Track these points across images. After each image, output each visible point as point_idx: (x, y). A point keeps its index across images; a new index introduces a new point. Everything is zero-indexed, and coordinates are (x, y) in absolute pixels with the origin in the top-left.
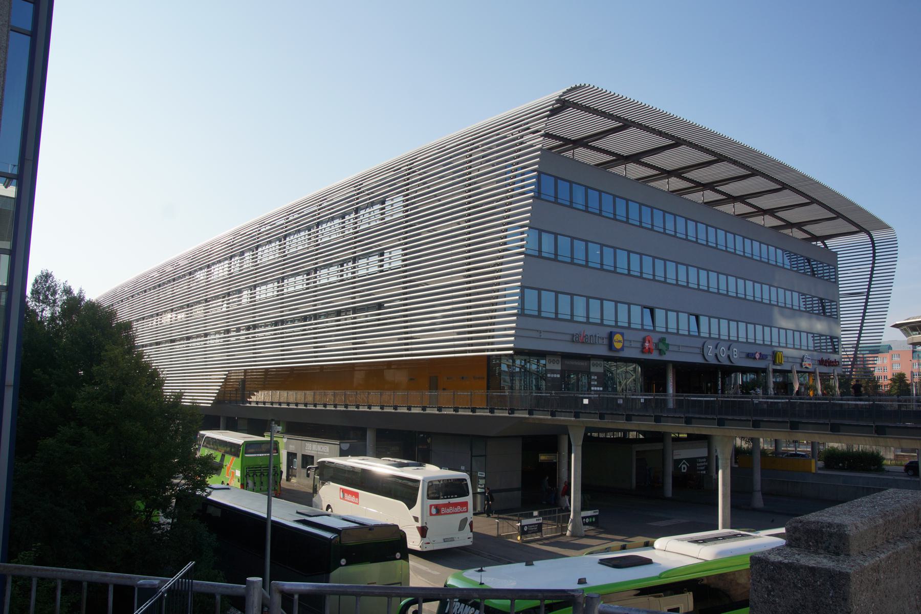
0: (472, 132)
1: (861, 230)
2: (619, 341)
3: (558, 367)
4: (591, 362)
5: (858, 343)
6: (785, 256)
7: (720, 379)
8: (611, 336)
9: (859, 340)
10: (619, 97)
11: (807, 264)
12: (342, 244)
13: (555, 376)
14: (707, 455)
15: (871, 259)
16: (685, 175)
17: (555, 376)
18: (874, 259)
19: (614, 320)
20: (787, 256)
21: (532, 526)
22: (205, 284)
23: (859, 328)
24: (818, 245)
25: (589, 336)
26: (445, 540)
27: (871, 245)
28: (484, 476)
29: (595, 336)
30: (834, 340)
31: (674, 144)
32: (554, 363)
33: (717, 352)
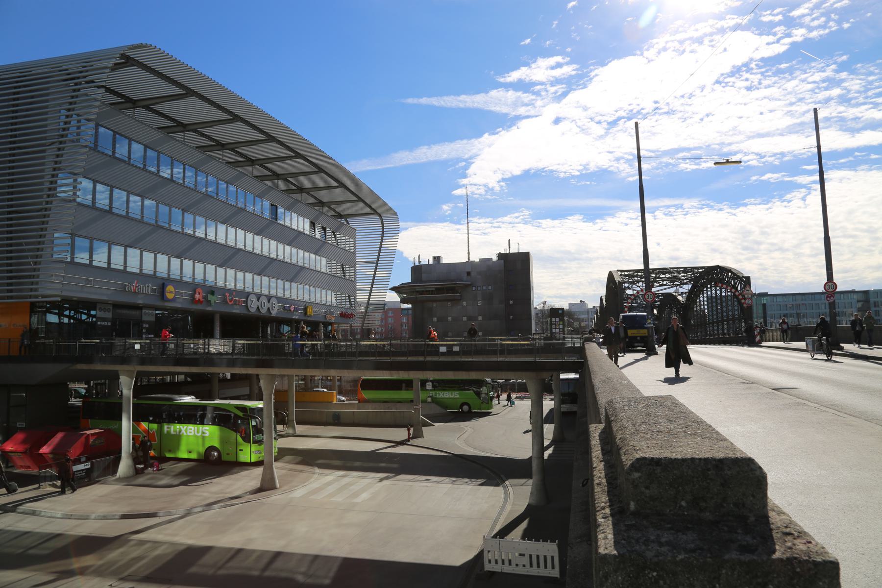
2: (171, 292)
3: (109, 315)
4: (143, 311)
7: (261, 328)
8: (163, 287)
9: (369, 298)
10: (184, 66)
11: (334, 239)
13: (106, 323)
14: (248, 393)
15: (381, 233)
17: (106, 323)
19: (107, 262)
20: (319, 231)
21: (80, 472)
23: (369, 289)
24: (342, 221)
26: (497, 231)
28: (24, 426)
30: (351, 298)
32: (105, 312)
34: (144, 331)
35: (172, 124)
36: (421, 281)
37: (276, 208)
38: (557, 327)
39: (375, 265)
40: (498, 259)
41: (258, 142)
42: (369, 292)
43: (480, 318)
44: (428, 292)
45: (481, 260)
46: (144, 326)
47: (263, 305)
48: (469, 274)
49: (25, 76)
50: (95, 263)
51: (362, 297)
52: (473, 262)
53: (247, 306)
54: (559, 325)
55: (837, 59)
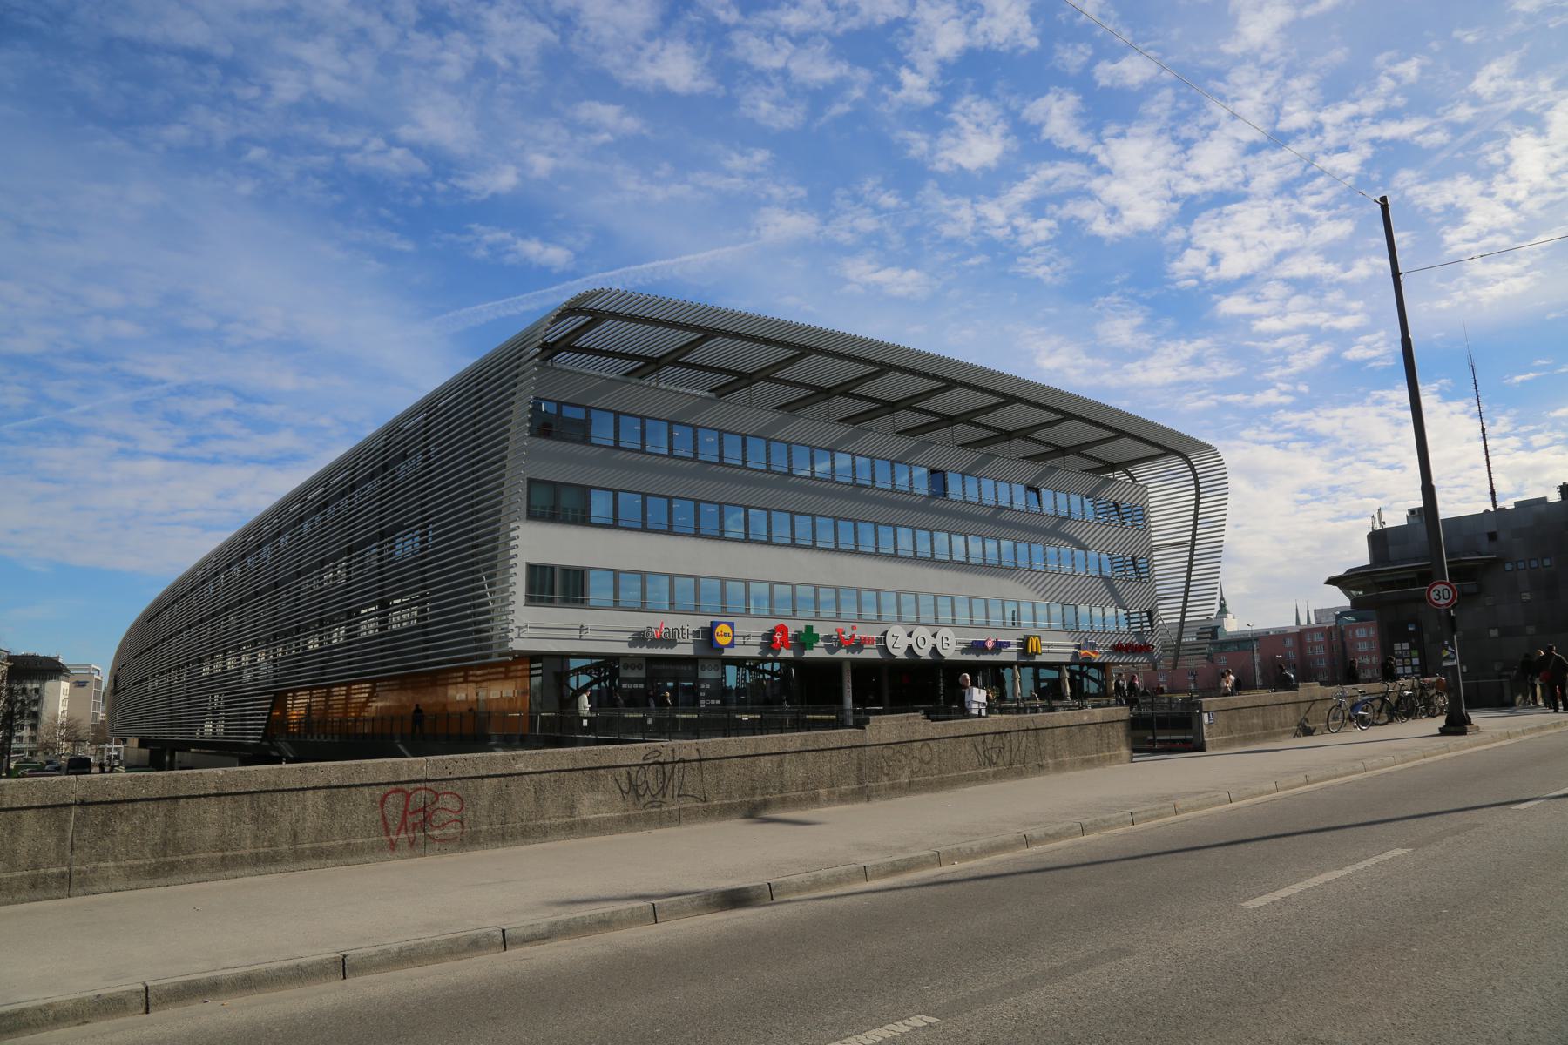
0: (498, 359)
1: (1167, 452)
5: (1182, 622)
6: (1086, 501)
12: (455, 469)
16: (855, 391)
17: (636, 686)
18: (1197, 499)
22: (378, 503)
23: (1182, 595)
25: (671, 631)
27: (1192, 477)
29: (682, 629)
31: (735, 380)
33: (912, 641)
34: (702, 694)
35: (730, 379)
36: (1390, 562)
37: (944, 476)
38: (1407, 662)
39: (1189, 548)
40: (1563, 498)
41: (860, 381)
42: (1182, 600)
43: (1531, 630)
44: (1403, 583)
45: (1520, 505)
46: (703, 686)
47: (921, 642)
48: (1492, 536)
49: (487, 372)
50: (971, 561)
51: (1169, 614)
52: (1503, 510)
53: (886, 647)
54: (1411, 658)
55: (1426, 131)
